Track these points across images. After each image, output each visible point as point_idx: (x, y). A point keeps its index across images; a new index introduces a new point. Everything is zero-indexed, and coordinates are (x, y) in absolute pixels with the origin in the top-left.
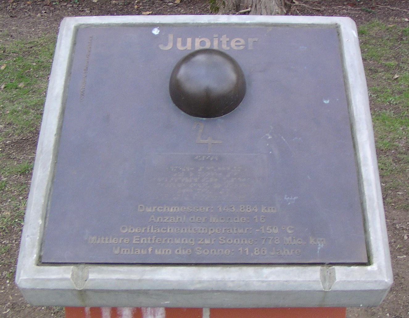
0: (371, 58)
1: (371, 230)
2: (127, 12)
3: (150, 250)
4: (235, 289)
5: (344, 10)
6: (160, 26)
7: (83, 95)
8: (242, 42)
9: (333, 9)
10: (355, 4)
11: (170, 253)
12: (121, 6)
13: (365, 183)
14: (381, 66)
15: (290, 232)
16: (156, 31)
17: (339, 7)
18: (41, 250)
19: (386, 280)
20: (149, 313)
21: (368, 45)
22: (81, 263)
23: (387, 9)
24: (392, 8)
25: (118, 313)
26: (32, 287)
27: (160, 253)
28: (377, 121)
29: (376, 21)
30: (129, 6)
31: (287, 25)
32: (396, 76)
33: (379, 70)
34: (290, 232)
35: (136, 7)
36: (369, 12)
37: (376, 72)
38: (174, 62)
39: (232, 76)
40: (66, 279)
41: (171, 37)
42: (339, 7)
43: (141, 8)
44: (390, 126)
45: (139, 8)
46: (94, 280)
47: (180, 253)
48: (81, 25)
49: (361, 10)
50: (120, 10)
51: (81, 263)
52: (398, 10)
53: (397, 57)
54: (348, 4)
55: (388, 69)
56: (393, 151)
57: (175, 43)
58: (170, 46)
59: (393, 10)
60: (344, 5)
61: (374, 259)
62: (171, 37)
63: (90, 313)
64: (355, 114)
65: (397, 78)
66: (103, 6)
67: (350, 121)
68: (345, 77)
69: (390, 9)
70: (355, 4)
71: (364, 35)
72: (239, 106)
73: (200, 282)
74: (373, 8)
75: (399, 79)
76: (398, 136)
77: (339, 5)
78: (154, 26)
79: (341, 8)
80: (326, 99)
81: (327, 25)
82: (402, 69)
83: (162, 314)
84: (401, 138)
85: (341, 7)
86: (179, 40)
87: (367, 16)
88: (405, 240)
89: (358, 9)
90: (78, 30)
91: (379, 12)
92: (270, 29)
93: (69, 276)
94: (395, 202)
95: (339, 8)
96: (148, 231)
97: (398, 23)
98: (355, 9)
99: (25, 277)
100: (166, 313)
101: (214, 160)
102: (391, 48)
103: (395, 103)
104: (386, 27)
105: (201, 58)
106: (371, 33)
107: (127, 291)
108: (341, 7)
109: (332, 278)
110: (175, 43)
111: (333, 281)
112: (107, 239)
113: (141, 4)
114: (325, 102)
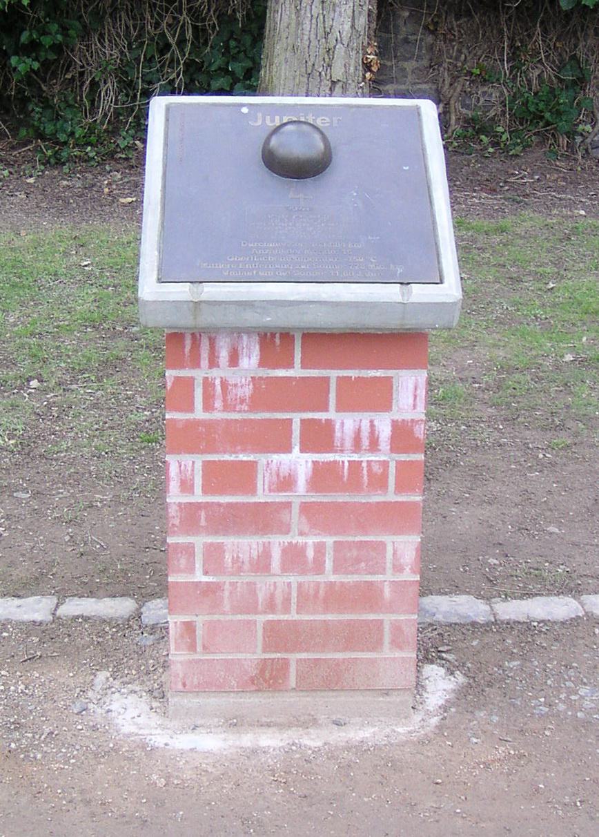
0: (514, 262)
1: (443, 260)
2: (91, 199)
3: (255, 272)
4: (328, 300)
5: (474, 199)
6: (249, 105)
7: (181, 161)
8: (328, 120)
9: (455, 196)
10: (495, 190)
11: (272, 274)
12: (80, 190)
13: (439, 228)
14: (530, 274)
15: (373, 261)
16: (245, 110)
17: (466, 193)
18: (158, 275)
19: (456, 294)
20: (245, 354)
21: (509, 247)
22: (195, 282)
23: (550, 197)
24: (560, 196)
25: (216, 354)
26: (154, 299)
27: (263, 274)
28: (512, 337)
29: (527, 213)
30: (94, 189)
31: (370, 107)
32: (551, 285)
33: (525, 279)
34: (373, 261)
35: (106, 190)
36: (518, 203)
37: (520, 281)
38: (265, 136)
39: (321, 146)
40: (184, 292)
41: (260, 115)
42: (466, 193)
43: (114, 192)
44: (531, 342)
45: (112, 192)
46: (209, 292)
47: (280, 274)
48: (171, 103)
49: (504, 199)
50: (78, 196)
51: (195, 282)
52: (570, 199)
53: (557, 262)
54: (481, 190)
55: (539, 277)
56: (533, 370)
57: (264, 120)
58: (259, 123)
59: (560, 199)
60: (475, 191)
61: (446, 280)
62: (260, 115)
63: (189, 354)
64: (432, 178)
65: (552, 289)
66: (46, 189)
67: (427, 183)
68: (424, 150)
69: (556, 197)
70: (495, 190)
71: (504, 233)
72: (327, 170)
73: (299, 294)
74: (526, 196)
75: (555, 289)
76: (543, 352)
77: (466, 191)
78: (243, 105)
79: (468, 195)
80: (406, 166)
81: (408, 106)
82: (562, 278)
83: (256, 356)
84: (548, 356)
85: (468, 193)
86: (268, 118)
87: (514, 207)
88: (541, 459)
89: (499, 196)
90: (168, 109)
91: (536, 202)
92: (354, 109)
93: (187, 289)
94: (529, 422)
95: (465, 195)
96: (252, 259)
97: (567, 217)
98: (493, 197)
99: (148, 291)
100: (261, 355)
101: (306, 210)
102: (548, 251)
103: (544, 316)
104: (546, 223)
105: (290, 127)
106: (518, 230)
107: (236, 302)
108: (468, 193)
109: (410, 292)
110: (264, 120)
111: (411, 295)
112: (217, 265)
113: (114, 187)
114: (405, 168)
